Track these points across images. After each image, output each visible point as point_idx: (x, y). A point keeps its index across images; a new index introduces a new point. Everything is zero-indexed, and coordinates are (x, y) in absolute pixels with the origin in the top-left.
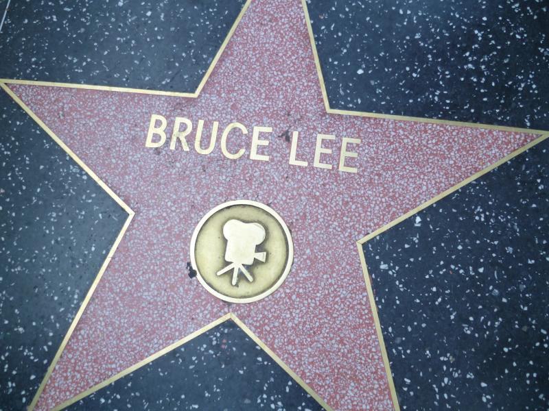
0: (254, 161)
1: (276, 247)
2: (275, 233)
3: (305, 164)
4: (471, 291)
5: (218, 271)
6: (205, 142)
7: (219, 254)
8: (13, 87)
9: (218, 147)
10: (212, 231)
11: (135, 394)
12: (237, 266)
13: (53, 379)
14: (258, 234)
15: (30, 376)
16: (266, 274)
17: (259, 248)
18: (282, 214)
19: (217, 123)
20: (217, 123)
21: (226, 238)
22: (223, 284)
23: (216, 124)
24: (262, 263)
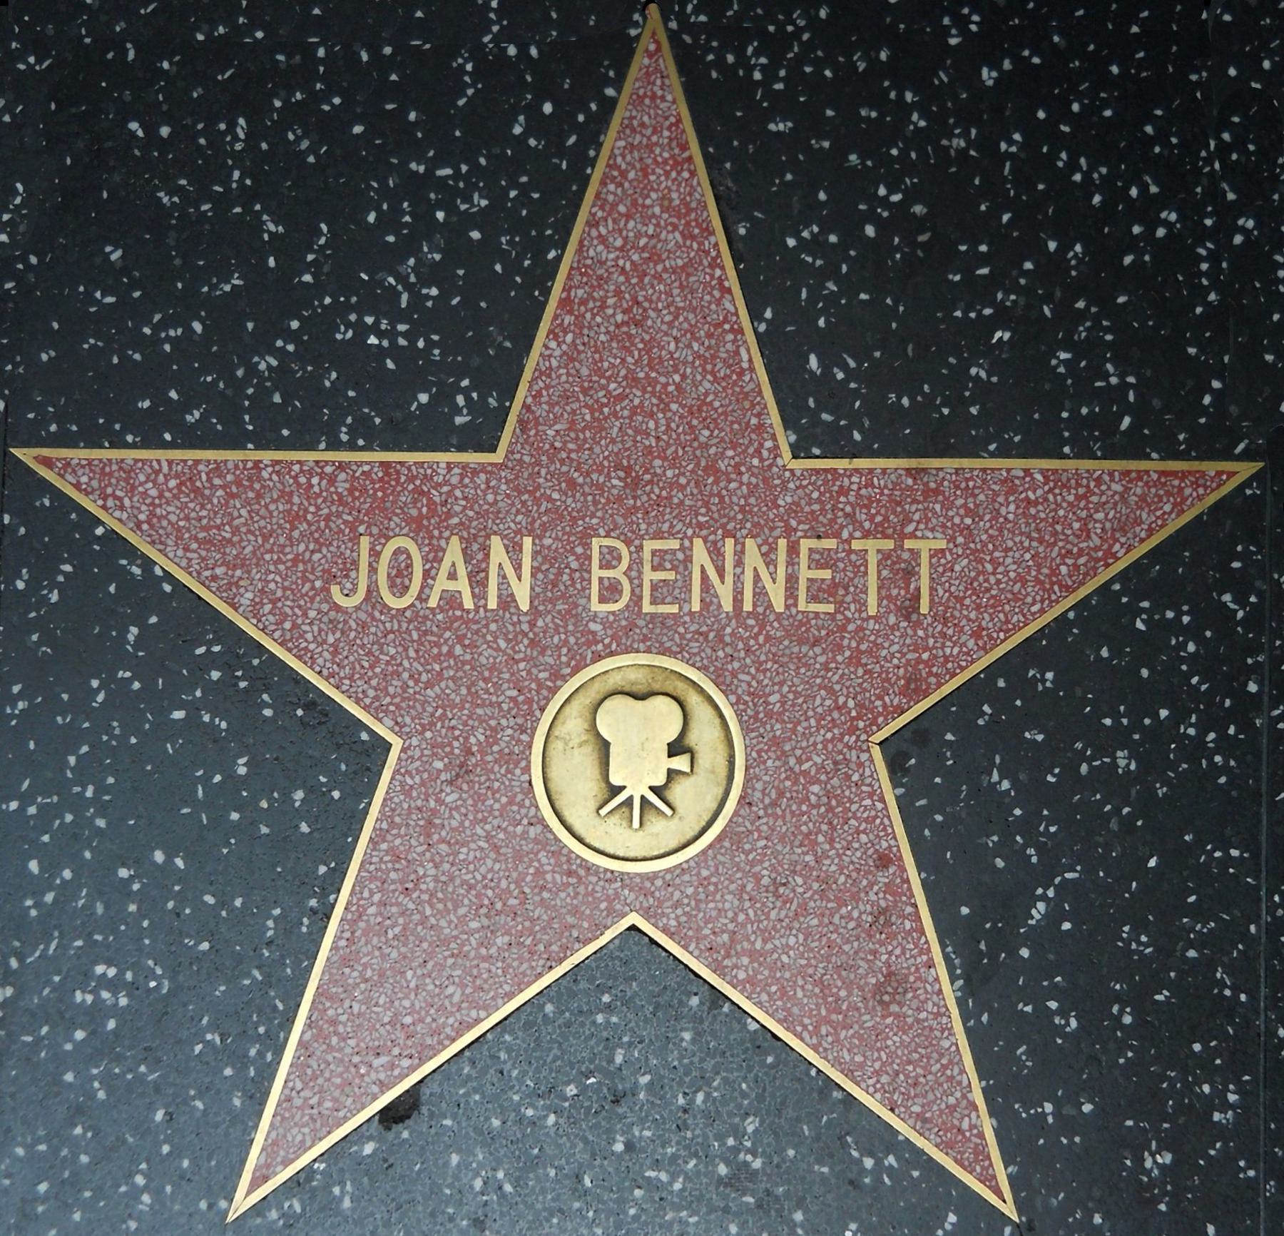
1: (705, 735)
2: (693, 699)
5: (601, 807)
8: (47, 462)
12: (637, 789)
13: (696, 232)
14: (663, 719)
15: (1020, 441)
16: (694, 798)
17: (675, 749)
18: (550, 836)
19: (489, 607)
20: (489, 607)
21: (606, 737)
22: (663, 832)
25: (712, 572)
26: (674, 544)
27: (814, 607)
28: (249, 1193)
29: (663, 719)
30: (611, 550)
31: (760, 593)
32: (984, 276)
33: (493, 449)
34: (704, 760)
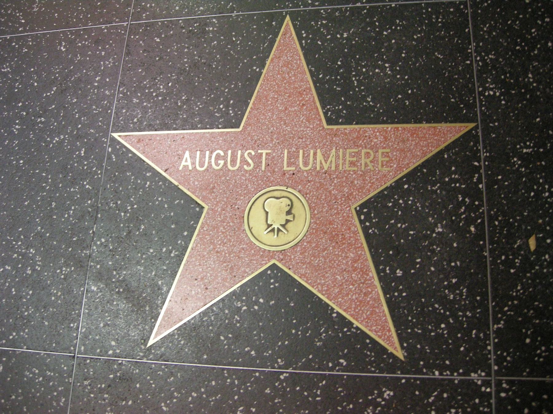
1: (298, 210)
4: (402, 204)
6: (233, 162)
7: (265, 220)
9: (210, 163)
17: (289, 213)
21: (281, 199)
23: (208, 153)
24: (291, 221)
27: (350, 169)
28: (154, 339)
30: (368, 153)
33: (238, 127)
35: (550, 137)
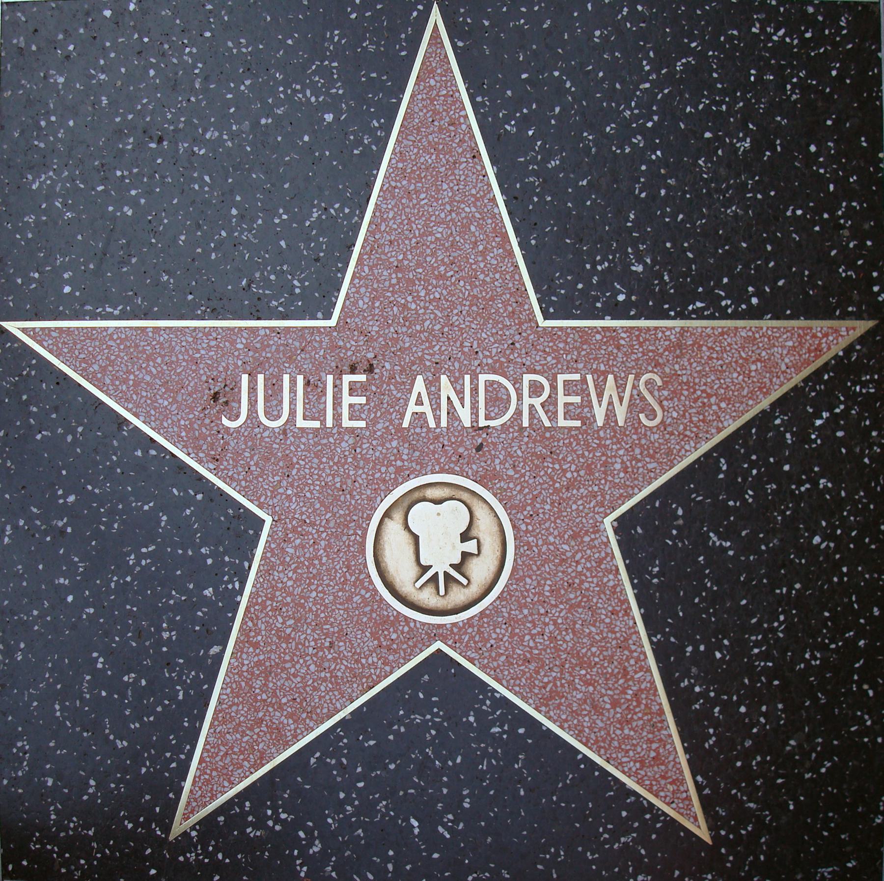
0: (302, 430)
1: (485, 527)
2: (481, 512)
3: (316, 424)
7: (413, 558)
10: (394, 527)
11: (274, 827)
14: (455, 515)
16: (480, 570)
17: (465, 537)
24: (472, 555)
25: (616, 399)
26: (577, 377)
29: (455, 515)
31: (452, 413)
32: (835, 188)
33: (547, 316)
34: (487, 548)
35: (255, 2)
